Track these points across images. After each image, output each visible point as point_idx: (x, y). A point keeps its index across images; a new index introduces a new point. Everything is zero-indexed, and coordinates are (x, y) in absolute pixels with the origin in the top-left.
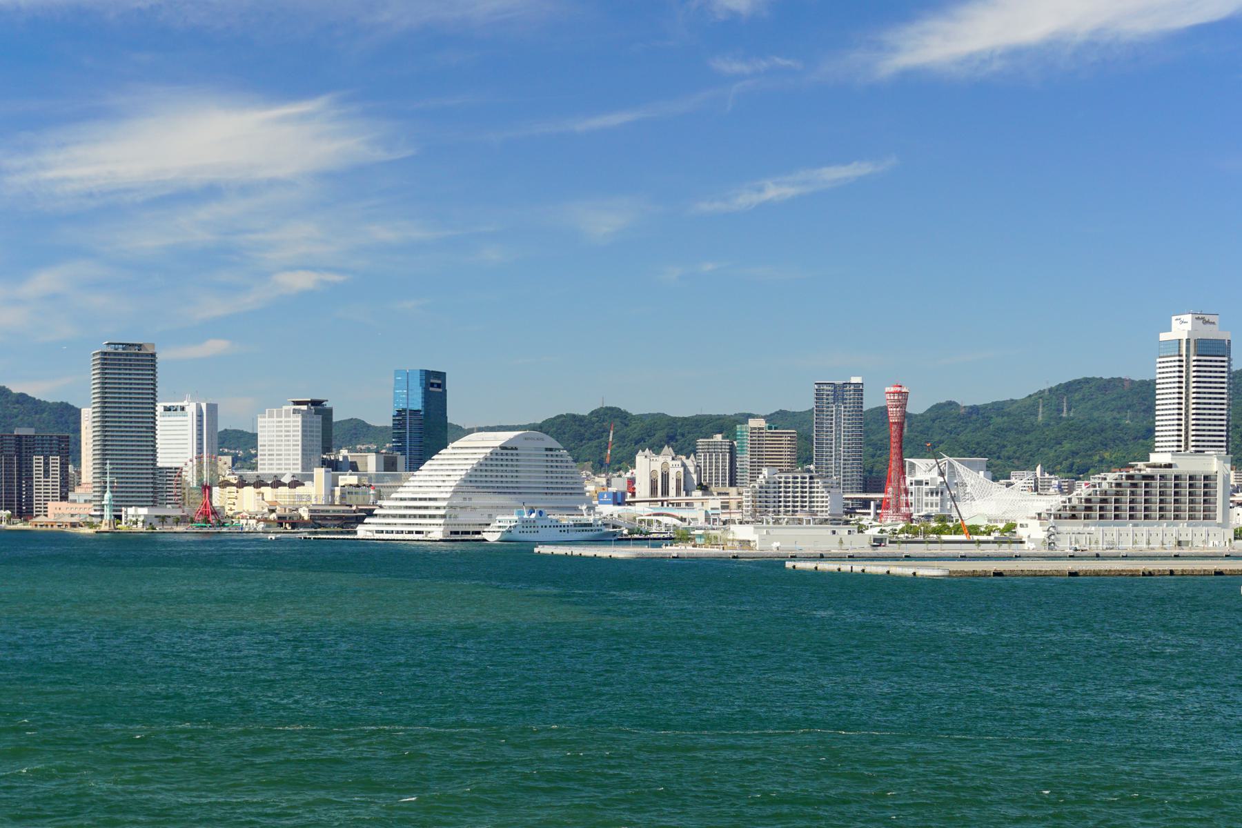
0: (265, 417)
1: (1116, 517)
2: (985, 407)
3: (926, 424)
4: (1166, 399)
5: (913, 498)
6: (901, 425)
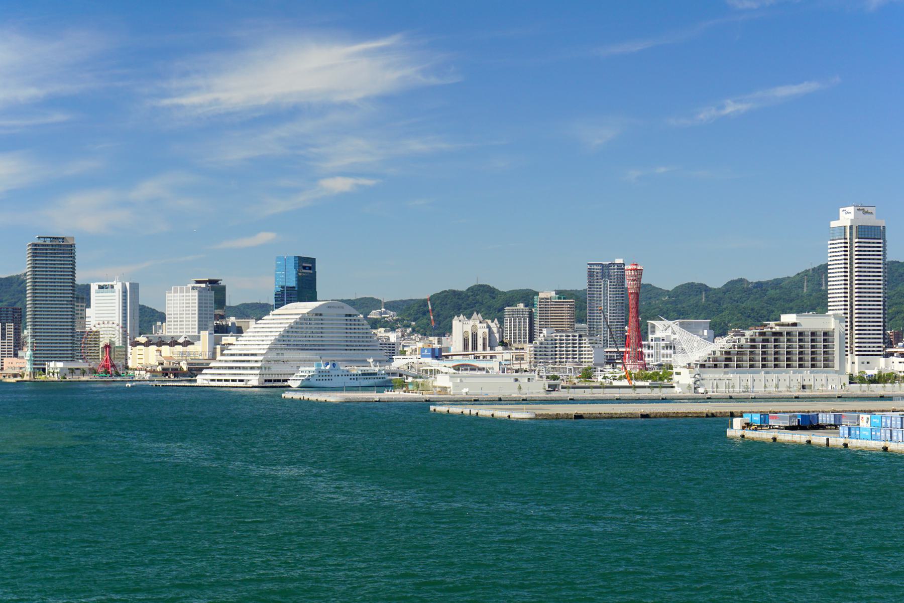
0: (171, 293)
1: (751, 366)
2: (767, 283)
3: (719, 295)
4: (836, 272)
5: (653, 351)
6: (637, 295)
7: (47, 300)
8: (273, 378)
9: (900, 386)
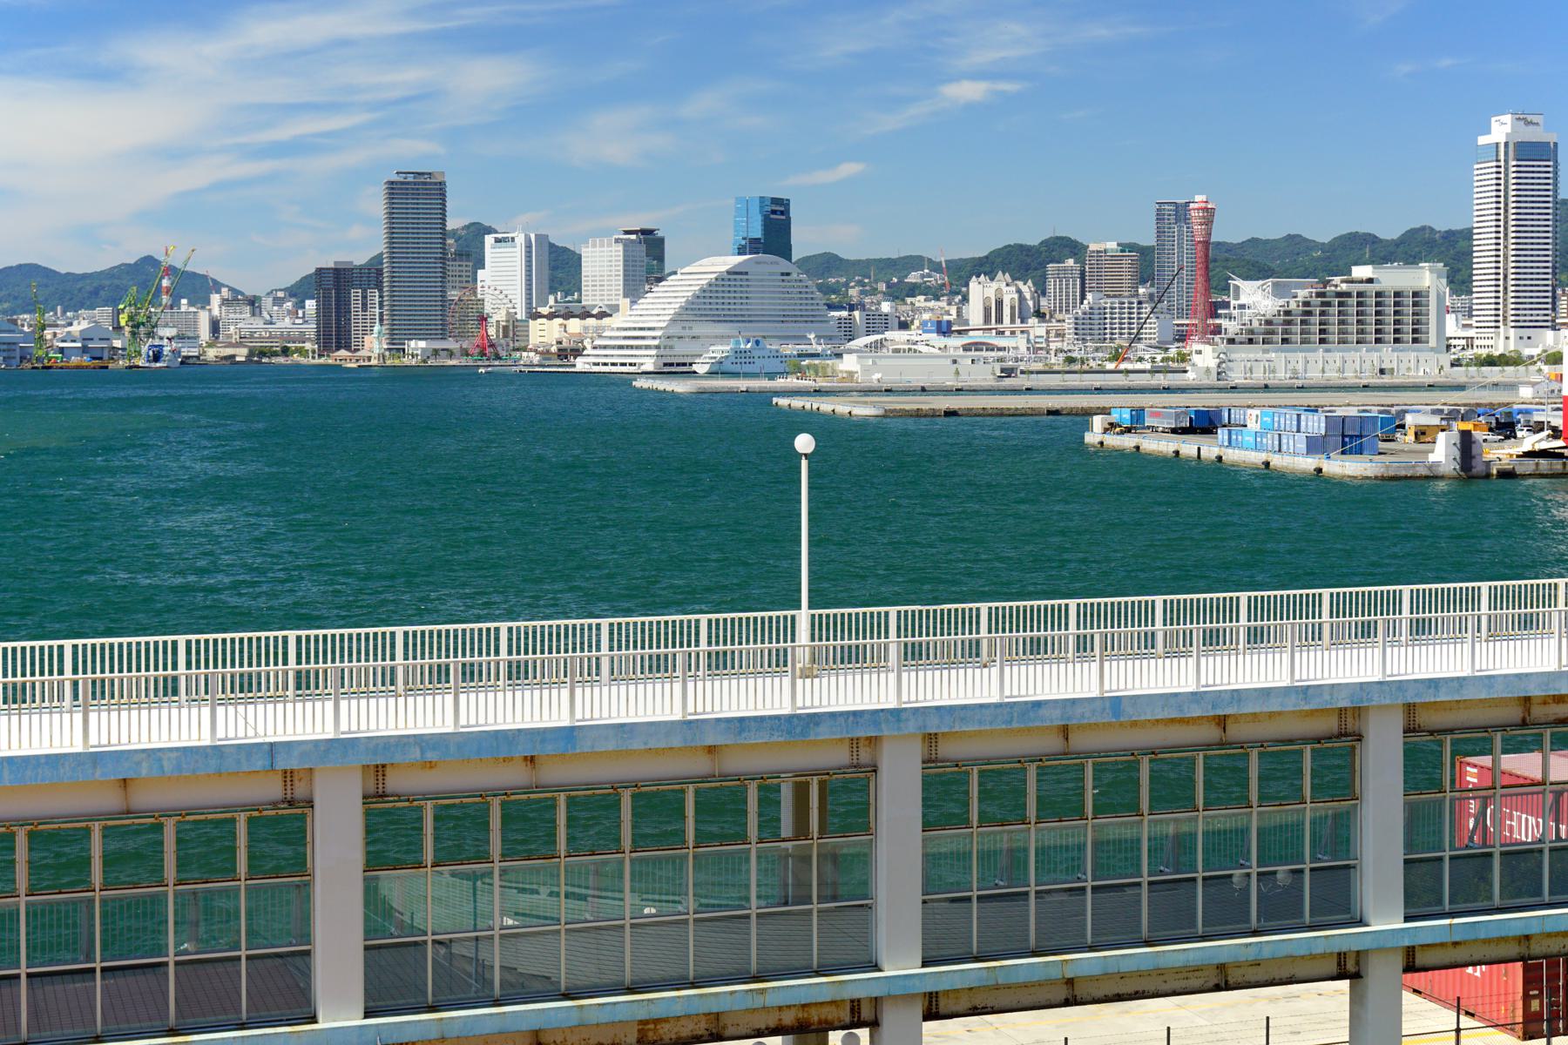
7: (408, 258)
8: (675, 361)
9: (1527, 370)
